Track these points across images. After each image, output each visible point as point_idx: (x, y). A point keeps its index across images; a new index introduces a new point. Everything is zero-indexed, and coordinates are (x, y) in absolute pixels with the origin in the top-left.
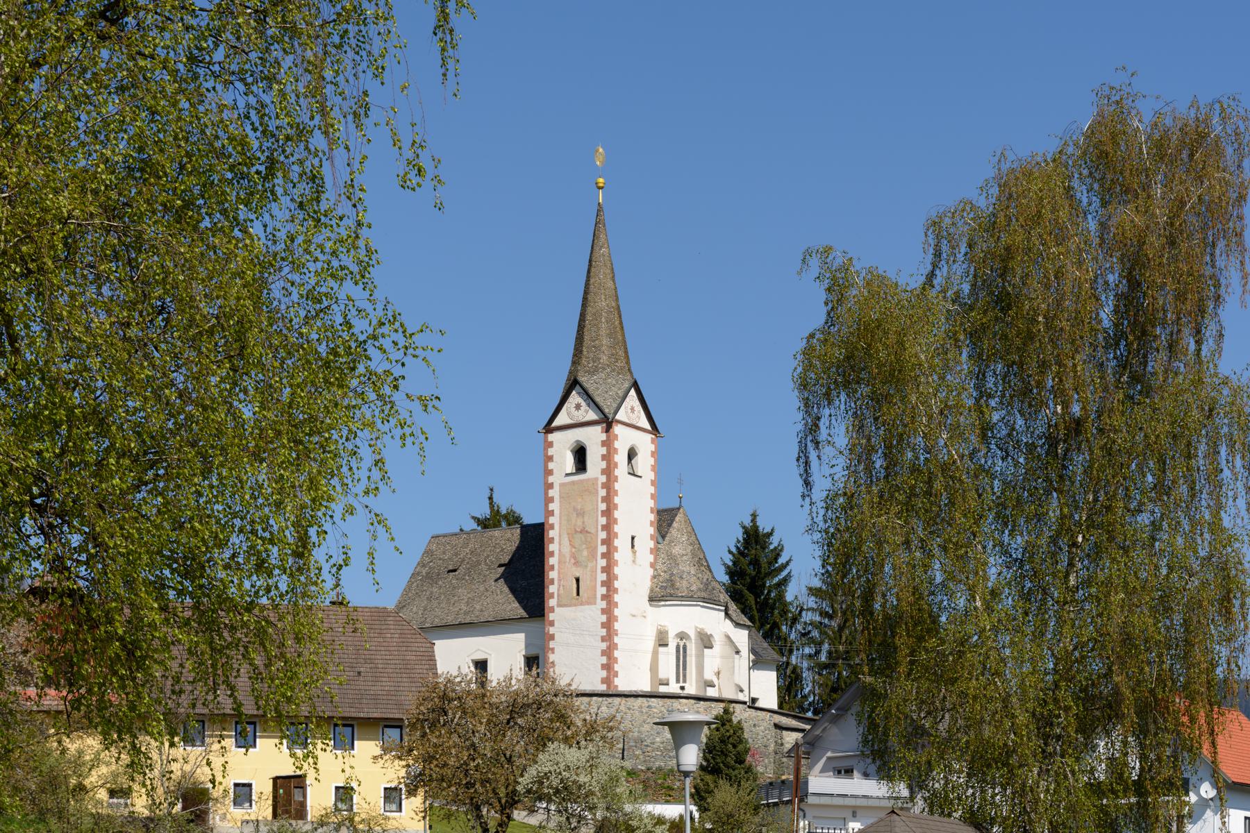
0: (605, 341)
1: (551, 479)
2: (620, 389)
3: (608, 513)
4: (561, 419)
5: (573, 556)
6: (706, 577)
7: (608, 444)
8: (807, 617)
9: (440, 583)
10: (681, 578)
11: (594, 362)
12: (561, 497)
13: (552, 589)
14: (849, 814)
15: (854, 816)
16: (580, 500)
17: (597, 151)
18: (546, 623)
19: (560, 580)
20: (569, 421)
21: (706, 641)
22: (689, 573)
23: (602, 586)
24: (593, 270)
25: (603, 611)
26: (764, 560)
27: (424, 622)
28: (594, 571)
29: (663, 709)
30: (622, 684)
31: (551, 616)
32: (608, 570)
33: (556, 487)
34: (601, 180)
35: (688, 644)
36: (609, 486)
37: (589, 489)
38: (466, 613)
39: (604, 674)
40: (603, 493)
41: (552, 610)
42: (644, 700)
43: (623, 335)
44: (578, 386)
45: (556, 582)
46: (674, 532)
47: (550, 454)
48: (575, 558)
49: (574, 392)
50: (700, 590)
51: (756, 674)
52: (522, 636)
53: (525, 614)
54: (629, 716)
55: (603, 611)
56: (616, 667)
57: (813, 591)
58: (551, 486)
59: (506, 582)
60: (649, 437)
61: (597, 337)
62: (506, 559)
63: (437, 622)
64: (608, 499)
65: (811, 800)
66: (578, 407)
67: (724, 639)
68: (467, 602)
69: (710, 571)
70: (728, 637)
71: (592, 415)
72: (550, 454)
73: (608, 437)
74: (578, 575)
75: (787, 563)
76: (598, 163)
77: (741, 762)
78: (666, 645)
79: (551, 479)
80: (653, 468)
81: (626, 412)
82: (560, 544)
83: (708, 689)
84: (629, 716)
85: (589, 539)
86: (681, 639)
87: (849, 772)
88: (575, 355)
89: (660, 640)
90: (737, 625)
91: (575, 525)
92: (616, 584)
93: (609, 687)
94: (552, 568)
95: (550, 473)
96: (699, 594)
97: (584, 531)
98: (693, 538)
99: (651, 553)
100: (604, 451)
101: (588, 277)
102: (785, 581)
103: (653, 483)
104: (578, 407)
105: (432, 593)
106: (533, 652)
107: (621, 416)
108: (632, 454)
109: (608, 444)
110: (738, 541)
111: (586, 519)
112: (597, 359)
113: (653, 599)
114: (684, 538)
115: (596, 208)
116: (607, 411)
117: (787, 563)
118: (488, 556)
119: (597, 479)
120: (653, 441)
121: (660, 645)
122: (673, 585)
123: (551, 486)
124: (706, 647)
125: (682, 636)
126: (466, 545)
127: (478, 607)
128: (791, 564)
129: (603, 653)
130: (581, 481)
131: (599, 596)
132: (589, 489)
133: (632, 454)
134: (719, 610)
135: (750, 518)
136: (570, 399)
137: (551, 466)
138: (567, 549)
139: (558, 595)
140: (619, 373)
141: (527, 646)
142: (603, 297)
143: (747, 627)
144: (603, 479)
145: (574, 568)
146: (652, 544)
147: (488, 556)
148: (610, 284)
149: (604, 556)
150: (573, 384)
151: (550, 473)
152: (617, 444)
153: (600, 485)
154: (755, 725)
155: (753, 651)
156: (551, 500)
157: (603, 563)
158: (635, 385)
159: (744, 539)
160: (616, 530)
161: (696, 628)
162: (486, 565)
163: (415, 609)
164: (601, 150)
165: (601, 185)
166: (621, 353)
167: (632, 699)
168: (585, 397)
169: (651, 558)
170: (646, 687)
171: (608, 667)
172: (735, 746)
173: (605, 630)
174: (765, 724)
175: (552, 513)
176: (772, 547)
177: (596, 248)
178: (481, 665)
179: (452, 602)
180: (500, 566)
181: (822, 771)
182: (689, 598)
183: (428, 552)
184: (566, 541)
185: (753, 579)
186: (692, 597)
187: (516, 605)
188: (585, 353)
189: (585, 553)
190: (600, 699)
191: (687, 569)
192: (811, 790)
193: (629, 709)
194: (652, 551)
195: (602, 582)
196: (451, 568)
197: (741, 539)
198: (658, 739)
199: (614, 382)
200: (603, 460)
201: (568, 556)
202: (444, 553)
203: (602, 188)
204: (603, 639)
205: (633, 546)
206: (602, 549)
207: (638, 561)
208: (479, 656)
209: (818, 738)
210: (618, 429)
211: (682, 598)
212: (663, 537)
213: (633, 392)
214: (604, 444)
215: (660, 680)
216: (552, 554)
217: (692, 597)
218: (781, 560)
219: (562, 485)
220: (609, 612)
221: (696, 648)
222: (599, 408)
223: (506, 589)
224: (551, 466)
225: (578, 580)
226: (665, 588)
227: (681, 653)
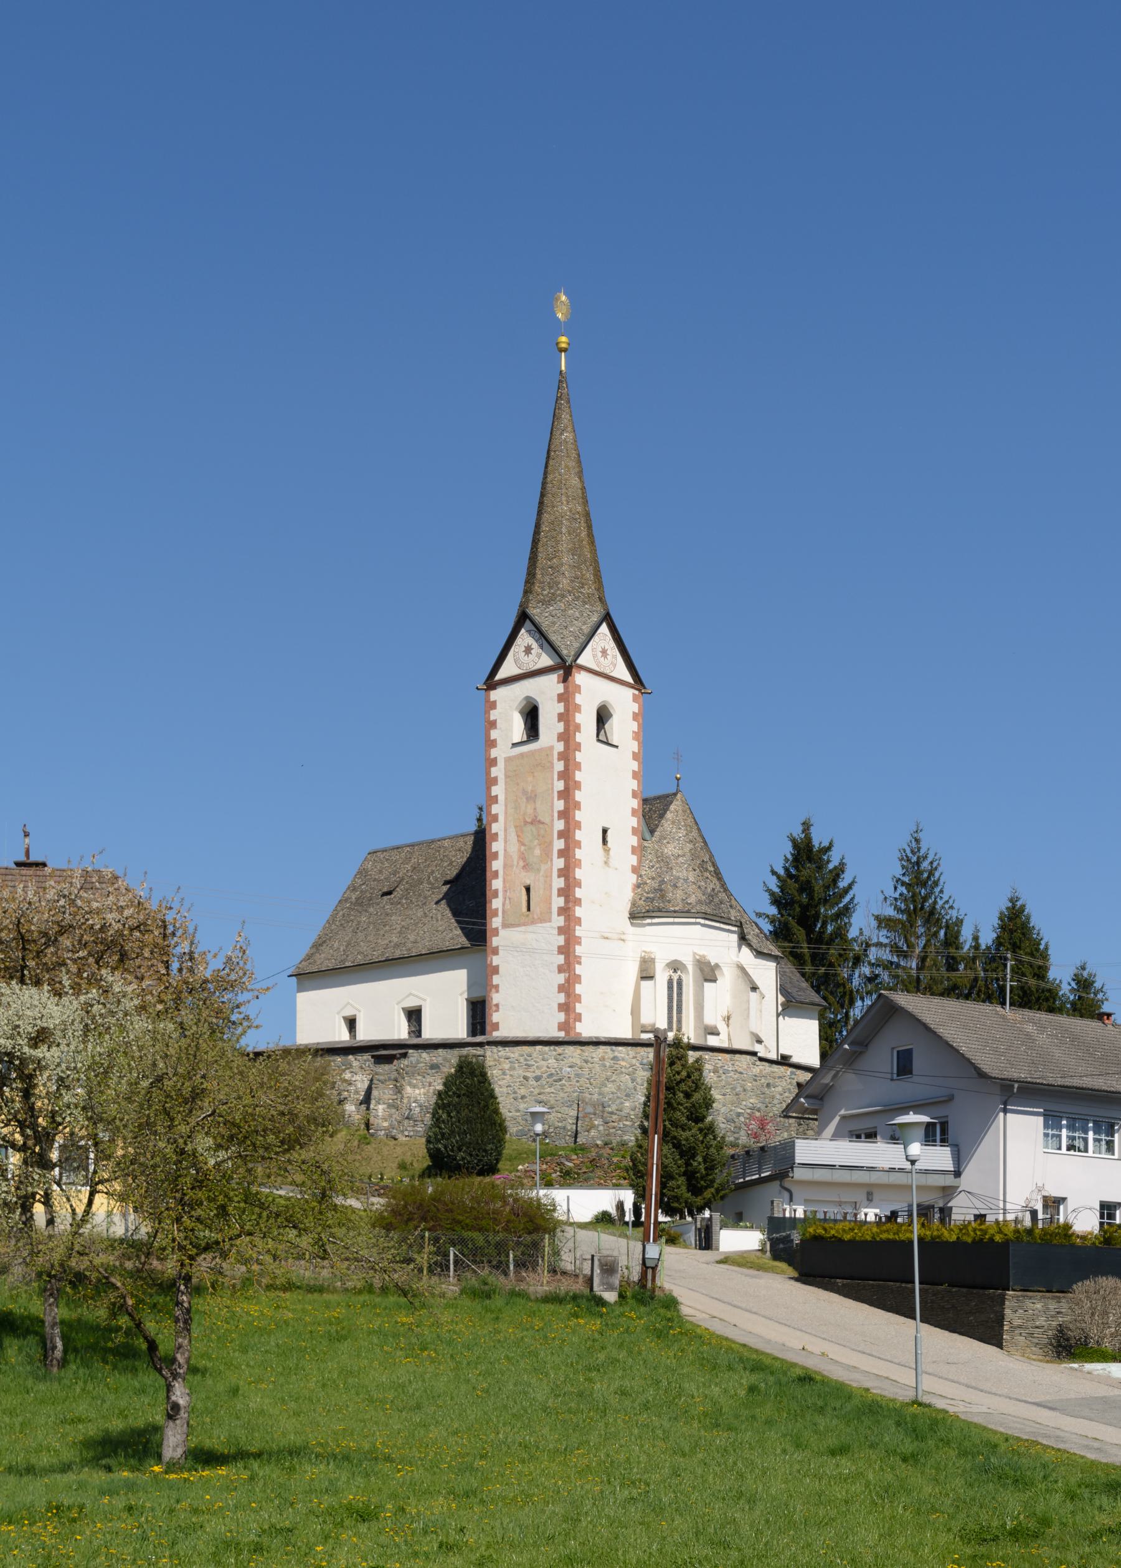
1: (494, 753)
2: (585, 623)
3: (566, 794)
5: (523, 857)
6: (712, 886)
7: (566, 698)
8: (873, 954)
9: (371, 910)
10: (675, 886)
11: (551, 588)
12: (507, 777)
13: (496, 904)
14: (861, 1196)
15: (870, 1199)
16: (530, 779)
17: (558, 298)
18: (489, 950)
19: (505, 891)
20: (517, 671)
21: (708, 973)
22: (686, 880)
23: (559, 895)
24: (551, 462)
25: (561, 931)
26: (818, 886)
27: (343, 961)
28: (549, 876)
29: (634, 1061)
30: (585, 1029)
31: (495, 941)
32: (566, 873)
33: (501, 763)
34: (564, 339)
35: (684, 977)
36: (569, 758)
37: (540, 763)
38: (397, 946)
39: (562, 1017)
40: (559, 766)
41: (496, 932)
42: (608, 1049)
43: (594, 552)
44: (528, 623)
45: (500, 894)
46: (667, 825)
48: (524, 859)
49: (523, 631)
50: (700, 902)
53: (467, 943)
54: (586, 1071)
55: (561, 931)
56: (579, 1008)
57: (883, 922)
58: (493, 762)
59: (449, 905)
60: (630, 693)
61: (556, 554)
62: (452, 873)
63: (360, 959)
64: (566, 775)
65: (799, 1174)
66: (528, 650)
67: (736, 972)
68: (400, 933)
69: (720, 879)
70: (742, 969)
71: (546, 661)
72: (492, 718)
73: (566, 688)
74: (528, 882)
75: (850, 887)
76: (560, 315)
77: (699, 1119)
78: (651, 978)
79: (494, 753)
80: (636, 735)
81: (594, 656)
82: (506, 842)
83: (709, 1037)
84: (586, 1071)
85: (542, 832)
86: (675, 971)
87: (871, 1136)
88: (527, 582)
90: (759, 954)
91: (525, 814)
92: (578, 893)
93: (567, 1033)
95: (493, 744)
97: (535, 821)
98: (695, 833)
99: (633, 852)
100: (561, 708)
101: (545, 473)
102: (846, 911)
103: (635, 756)
104: (528, 650)
105: (359, 923)
106: (477, 994)
108: (603, 717)
109: (566, 698)
110: (786, 860)
112: (554, 584)
114: (682, 833)
115: (557, 377)
116: (564, 652)
117: (850, 887)
118: (433, 872)
119: (551, 748)
120: (635, 699)
122: (663, 897)
124: (706, 980)
125: (676, 966)
126: (407, 860)
127: (412, 938)
128: (855, 888)
129: (561, 989)
131: (555, 910)
132: (540, 763)
133: (603, 717)
135: (801, 828)
137: (494, 734)
138: (514, 848)
140: (585, 603)
142: (564, 498)
143: (775, 958)
144: (560, 747)
145: (523, 874)
146: (634, 841)
147: (433, 872)
148: (575, 481)
150: (523, 618)
153: (556, 756)
154: (768, 1085)
155: (783, 990)
156: (495, 781)
157: (559, 863)
158: (607, 618)
161: (695, 954)
162: (429, 883)
163: (336, 945)
165: (563, 345)
166: (589, 576)
167: (591, 1048)
168: (537, 635)
169: (634, 860)
170: (626, 1034)
172: (688, 1096)
173: (562, 957)
175: (495, 799)
176: (831, 866)
177: (557, 433)
178: (414, 1015)
179: (382, 932)
181: (836, 1136)
182: (686, 913)
183: (362, 873)
184: (513, 837)
185: (805, 908)
186: (688, 912)
188: (539, 576)
189: (537, 852)
190: (546, 1048)
191: (683, 874)
193: (586, 1062)
194: (634, 850)
195: (559, 890)
196: (385, 890)
197: (790, 857)
198: (627, 1104)
199: (577, 614)
201: (515, 857)
202: (380, 872)
203: (565, 350)
204: (561, 969)
205: (605, 841)
206: (559, 844)
207: (612, 862)
208: (411, 1003)
210: (580, 678)
211: (675, 914)
212: (652, 832)
213: (604, 628)
214: (561, 698)
215: (643, 1026)
217: (688, 912)
218: (842, 884)
219: (508, 760)
220: (568, 932)
221: (695, 981)
222: (554, 650)
224: (494, 734)
225: (528, 889)
226: (652, 900)
227: (675, 989)
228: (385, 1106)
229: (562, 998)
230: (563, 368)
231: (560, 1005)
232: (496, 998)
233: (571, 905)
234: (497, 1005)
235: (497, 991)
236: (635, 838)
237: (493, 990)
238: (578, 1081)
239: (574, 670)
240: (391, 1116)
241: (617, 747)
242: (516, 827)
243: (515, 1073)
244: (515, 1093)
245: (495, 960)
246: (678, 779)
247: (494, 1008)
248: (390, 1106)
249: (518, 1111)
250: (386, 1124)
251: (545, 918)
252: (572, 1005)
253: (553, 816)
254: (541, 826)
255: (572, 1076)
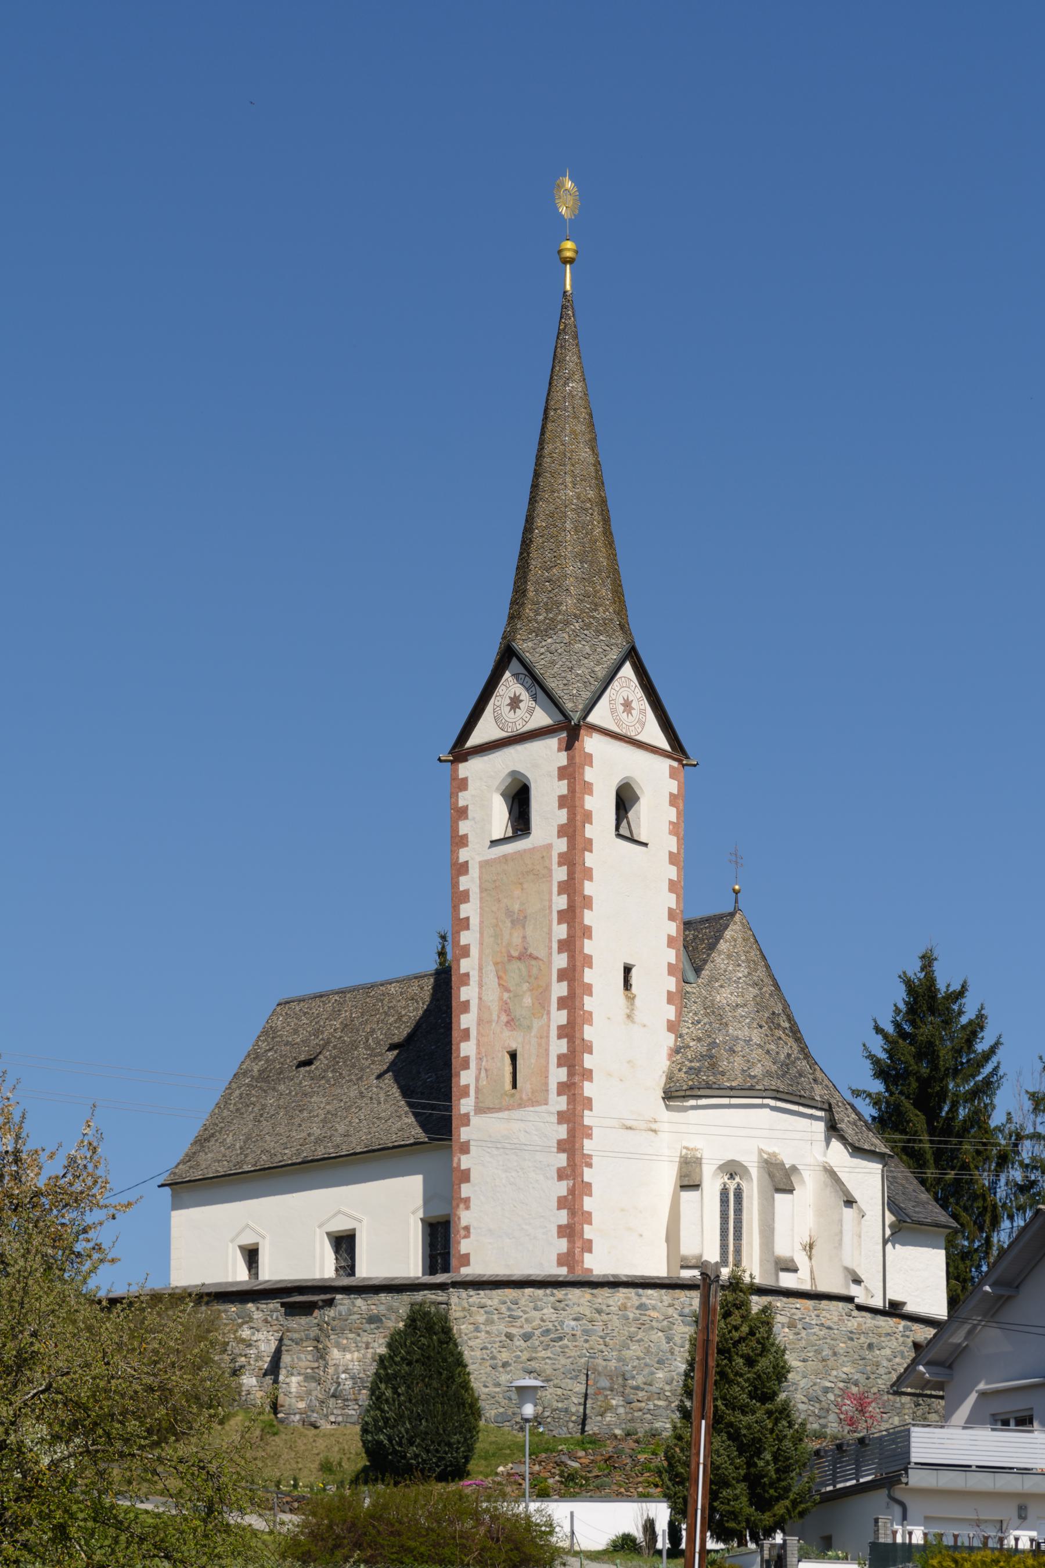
0: (572, 568)
1: (464, 855)
2: (599, 663)
3: (571, 916)
4: (484, 731)
6: (786, 1050)
7: (570, 773)
10: (732, 1051)
11: (548, 611)
12: (482, 890)
13: (466, 1078)
14: (1009, 1512)
16: (517, 893)
17: (561, 186)
18: (455, 1147)
19: (480, 1059)
20: (497, 734)
22: (748, 1041)
25: (562, 1117)
29: (670, 1311)
31: (464, 1134)
32: (570, 1031)
33: (474, 871)
34: (569, 245)
35: (744, 1186)
36: (572, 860)
38: (318, 1141)
39: (563, 1245)
40: (560, 874)
41: (466, 1120)
42: (631, 1292)
43: (613, 557)
45: (473, 1064)
46: (719, 960)
47: (461, 803)
48: (508, 1012)
49: (507, 674)
50: (769, 1074)
51: (899, 1253)
52: (419, 1179)
53: (423, 1137)
54: (599, 1327)
55: (562, 1117)
56: (588, 1232)
58: (463, 868)
59: (397, 1080)
60: (665, 765)
61: (556, 561)
62: (401, 1033)
63: (265, 1160)
64: (571, 887)
65: (916, 1478)
67: (823, 1177)
68: (324, 1121)
70: (831, 1173)
71: (541, 718)
72: (461, 803)
73: (571, 759)
74: (513, 1046)
75: (993, 1050)
76: (563, 210)
77: (767, 1397)
78: (696, 1187)
79: (464, 855)
81: (613, 711)
82: (481, 986)
84: (599, 1327)
85: (535, 971)
86: (732, 1177)
88: (514, 602)
89: (682, 1175)
90: (857, 1151)
92: (588, 1061)
94: (466, 1035)
96: (766, 1082)
97: (525, 956)
98: (761, 972)
100: (562, 787)
101: (541, 443)
102: (988, 1087)
103: (673, 859)
107: (598, 716)
109: (570, 773)
110: (897, 1011)
111: (529, 931)
113: (672, 1095)
114: (742, 972)
115: (560, 301)
116: (569, 705)
117: (993, 1050)
118: (373, 1031)
119: (549, 847)
120: (673, 774)
121: (684, 1187)
122: (713, 1066)
123: (463, 868)
124: (779, 1190)
125: (732, 1169)
126: (335, 1013)
127: (341, 1128)
129: (562, 1203)
130: (520, 854)
131: (553, 1087)
134: (811, 1117)
135: (919, 964)
136: (501, 689)
137: (464, 827)
138: (493, 995)
139: (478, 1090)
140: (599, 633)
141: (427, 1201)
142: (568, 479)
144: (561, 845)
145: (507, 1033)
146: (671, 984)
147: (373, 1031)
149: (563, 1003)
150: (507, 655)
151: (462, 841)
152: (589, 775)
153: (555, 859)
155: (892, 1204)
156: (465, 897)
157: (560, 1017)
158: (632, 655)
159: (907, 1003)
160: (587, 950)
161: (761, 1151)
164: (569, 184)
165: (569, 254)
166: (606, 593)
167: (606, 1292)
168: (529, 681)
170: (659, 1270)
171: (570, 1231)
172: (750, 1362)
174: (894, 1344)
176: (964, 1020)
177: (558, 383)
180: (392, 1047)
181: (972, 1422)
183: (269, 1033)
184: (491, 980)
186: (751, 1088)
187: (411, 1119)
188: (531, 594)
189: (528, 1001)
190: (540, 1292)
191: (743, 1033)
192: (916, 1456)
193: (599, 1312)
194: (671, 998)
197: (902, 1006)
198: (660, 1375)
199: (588, 649)
200: (561, 806)
201: (495, 1008)
202: (296, 1032)
203: (571, 261)
204: (561, 1175)
205: (627, 985)
206: (560, 989)
207: (638, 1016)
208: (340, 1225)
209: (959, 1353)
210: (591, 743)
211: (732, 1092)
212: (698, 971)
213: (627, 670)
214: (563, 773)
215: (684, 1258)
216: (466, 1006)
218: (981, 1047)
219: (484, 865)
221: (761, 1192)
222: (553, 701)
223: (396, 1092)
224: (464, 827)
225: (513, 1056)
226: (698, 1071)
228: (300, 1378)
229: (563, 1217)
230: (568, 287)
231: (560, 1227)
232: (465, 1217)
233: (577, 1079)
234: (467, 1228)
235: (468, 1208)
236: (673, 980)
237: (462, 1206)
238: (586, 1341)
239: (582, 732)
240: (309, 1393)
241: (645, 845)
242: (496, 964)
243: (494, 1329)
244: (493, 1358)
245: (465, 1162)
246: (736, 892)
247: (463, 1233)
248: (307, 1378)
249: (498, 1385)
250: (302, 1405)
251: (539, 1099)
252: (578, 1227)
253: (551, 948)
254: (533, 962)
255: (579, 1333)
